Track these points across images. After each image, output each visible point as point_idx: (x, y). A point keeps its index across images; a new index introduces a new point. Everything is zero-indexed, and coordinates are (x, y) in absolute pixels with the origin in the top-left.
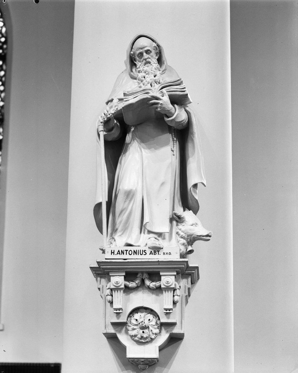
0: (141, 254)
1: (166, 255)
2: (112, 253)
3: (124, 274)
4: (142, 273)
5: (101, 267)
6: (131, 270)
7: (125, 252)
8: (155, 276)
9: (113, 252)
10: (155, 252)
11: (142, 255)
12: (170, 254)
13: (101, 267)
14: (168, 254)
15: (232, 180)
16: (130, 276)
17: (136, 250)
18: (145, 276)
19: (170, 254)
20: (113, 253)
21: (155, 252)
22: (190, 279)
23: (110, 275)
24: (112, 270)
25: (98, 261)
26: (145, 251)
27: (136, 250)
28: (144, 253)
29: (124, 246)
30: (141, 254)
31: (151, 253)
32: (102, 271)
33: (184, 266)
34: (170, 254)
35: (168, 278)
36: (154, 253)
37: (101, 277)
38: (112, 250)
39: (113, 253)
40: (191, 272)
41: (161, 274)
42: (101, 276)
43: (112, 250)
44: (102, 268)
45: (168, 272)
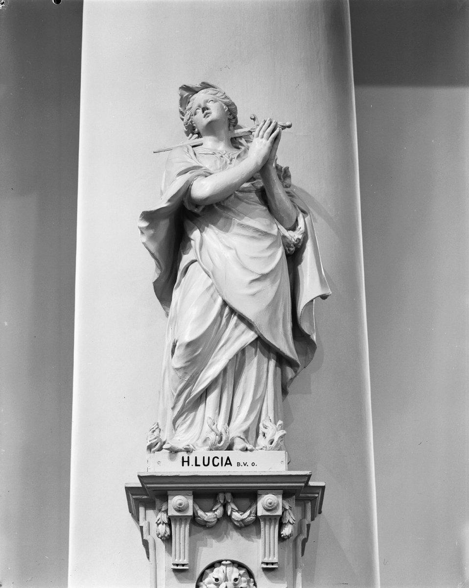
0: (206, 463)
2: (183, 461)
4: (224, 491)
5: (148, 485)
7: (200, 462)
8: (252, 496)
13: (148, 485)
18: (229, 497)
22: (309, 505)
30: (206, 463)
31: (228, 462)
32: (148, 494)
33: (303, 484)
38: (204, 457)
40: (309, 495)
43: (204, 457)
44: (148, 488)
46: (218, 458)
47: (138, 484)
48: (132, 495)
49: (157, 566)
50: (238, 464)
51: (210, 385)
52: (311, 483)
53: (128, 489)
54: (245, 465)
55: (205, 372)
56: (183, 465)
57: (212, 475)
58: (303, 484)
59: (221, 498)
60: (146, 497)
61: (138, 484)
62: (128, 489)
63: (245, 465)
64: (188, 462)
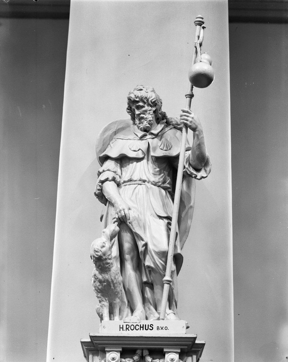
0: (147, 329)
1: (160, 331)
2: (120, 328)
3: (121, 350)
4: (142, 350)
5: (95, 342)
6: (129, 346)
9: (121, 327)
10: (158, 327)
11: (148, 330)
12: (166, 328)
13: (95, 342)
14: (164, 328)
15: (233, 285)
16: (125, 353)
17: (143, 325)
18: (146, 352)
19: (166, 328)
20: (121, 328)
21: (158, 327)
22: (195, 357)
23: (106, 349)
24: (107, 346)
25: (83, 340)
26: (151, 326)
27: (143, 325)
28: (150, 327)
29: (180, 152)
30: (147, 329)
34: (166, 328)
35: (172, 355)
36: (127, 328)
37: (93, 355)
39: (121, 328)
41: (165, 350)
42: (94, 352)
45: (177, 349)
46: (138, 326)
47: (89, 340)
48: (85, 346)
49: (32, 22)
50: (158, 328)
51: (162, 296)
52: (197, 342)
53: (82, 343)
54: (162, 329)
55: (107, 312)
56: (123, 325)
57: (101, 335)
58: (191, 343)
59: (139, 352)
60: (93, 348)
61: (89, 340)
62: (82, 343)
63: (162, 329)
64: (123, 328)
